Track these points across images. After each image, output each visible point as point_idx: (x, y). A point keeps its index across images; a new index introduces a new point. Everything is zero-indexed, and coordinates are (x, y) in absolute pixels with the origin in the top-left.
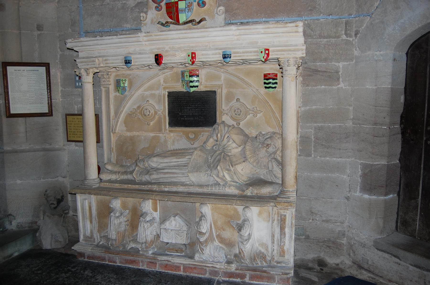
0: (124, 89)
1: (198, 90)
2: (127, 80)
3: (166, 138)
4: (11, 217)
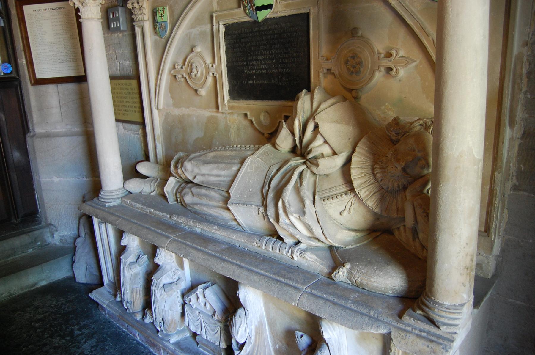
0: (163, 25)
1: (272, 16)
2: (167, 8)
3: (226, 122)
4: (52, 227)
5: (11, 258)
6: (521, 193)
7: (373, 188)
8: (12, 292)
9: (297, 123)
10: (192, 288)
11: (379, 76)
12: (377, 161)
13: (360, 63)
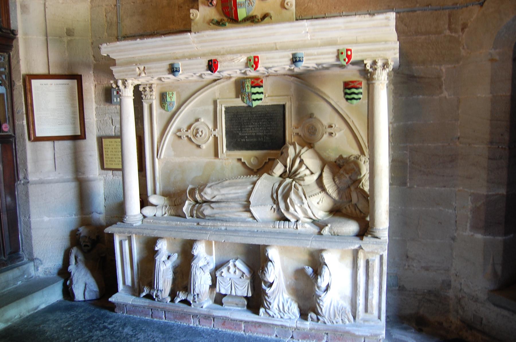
1: (261, 104)
2: (175, 93)
5: (6, 290)
6: (394, 186)
7: (335, 188)
8: (22, 314)
9: (288, 160)
10: (218, 267)
11: (326, 136)
12: (334, 175)
13: (316, 130)
